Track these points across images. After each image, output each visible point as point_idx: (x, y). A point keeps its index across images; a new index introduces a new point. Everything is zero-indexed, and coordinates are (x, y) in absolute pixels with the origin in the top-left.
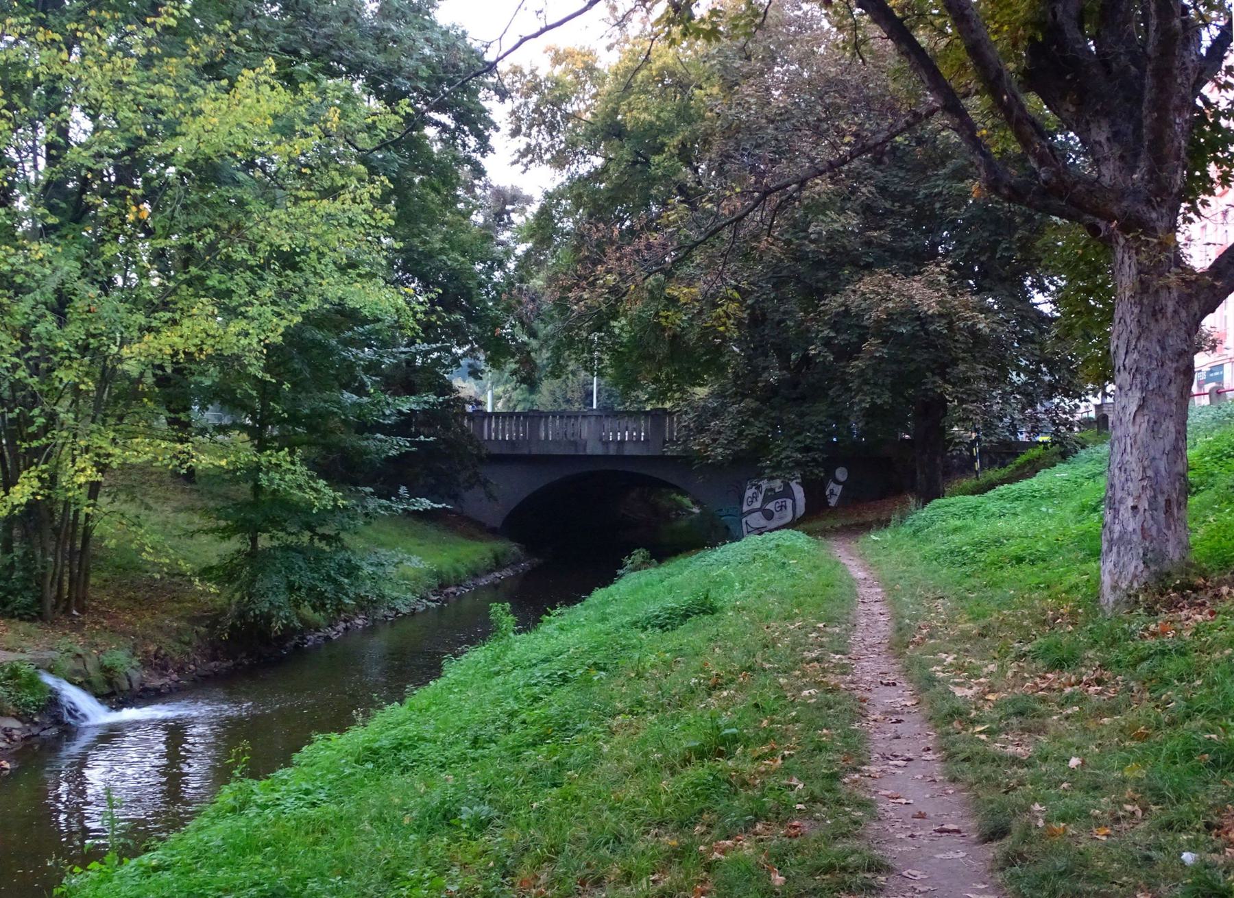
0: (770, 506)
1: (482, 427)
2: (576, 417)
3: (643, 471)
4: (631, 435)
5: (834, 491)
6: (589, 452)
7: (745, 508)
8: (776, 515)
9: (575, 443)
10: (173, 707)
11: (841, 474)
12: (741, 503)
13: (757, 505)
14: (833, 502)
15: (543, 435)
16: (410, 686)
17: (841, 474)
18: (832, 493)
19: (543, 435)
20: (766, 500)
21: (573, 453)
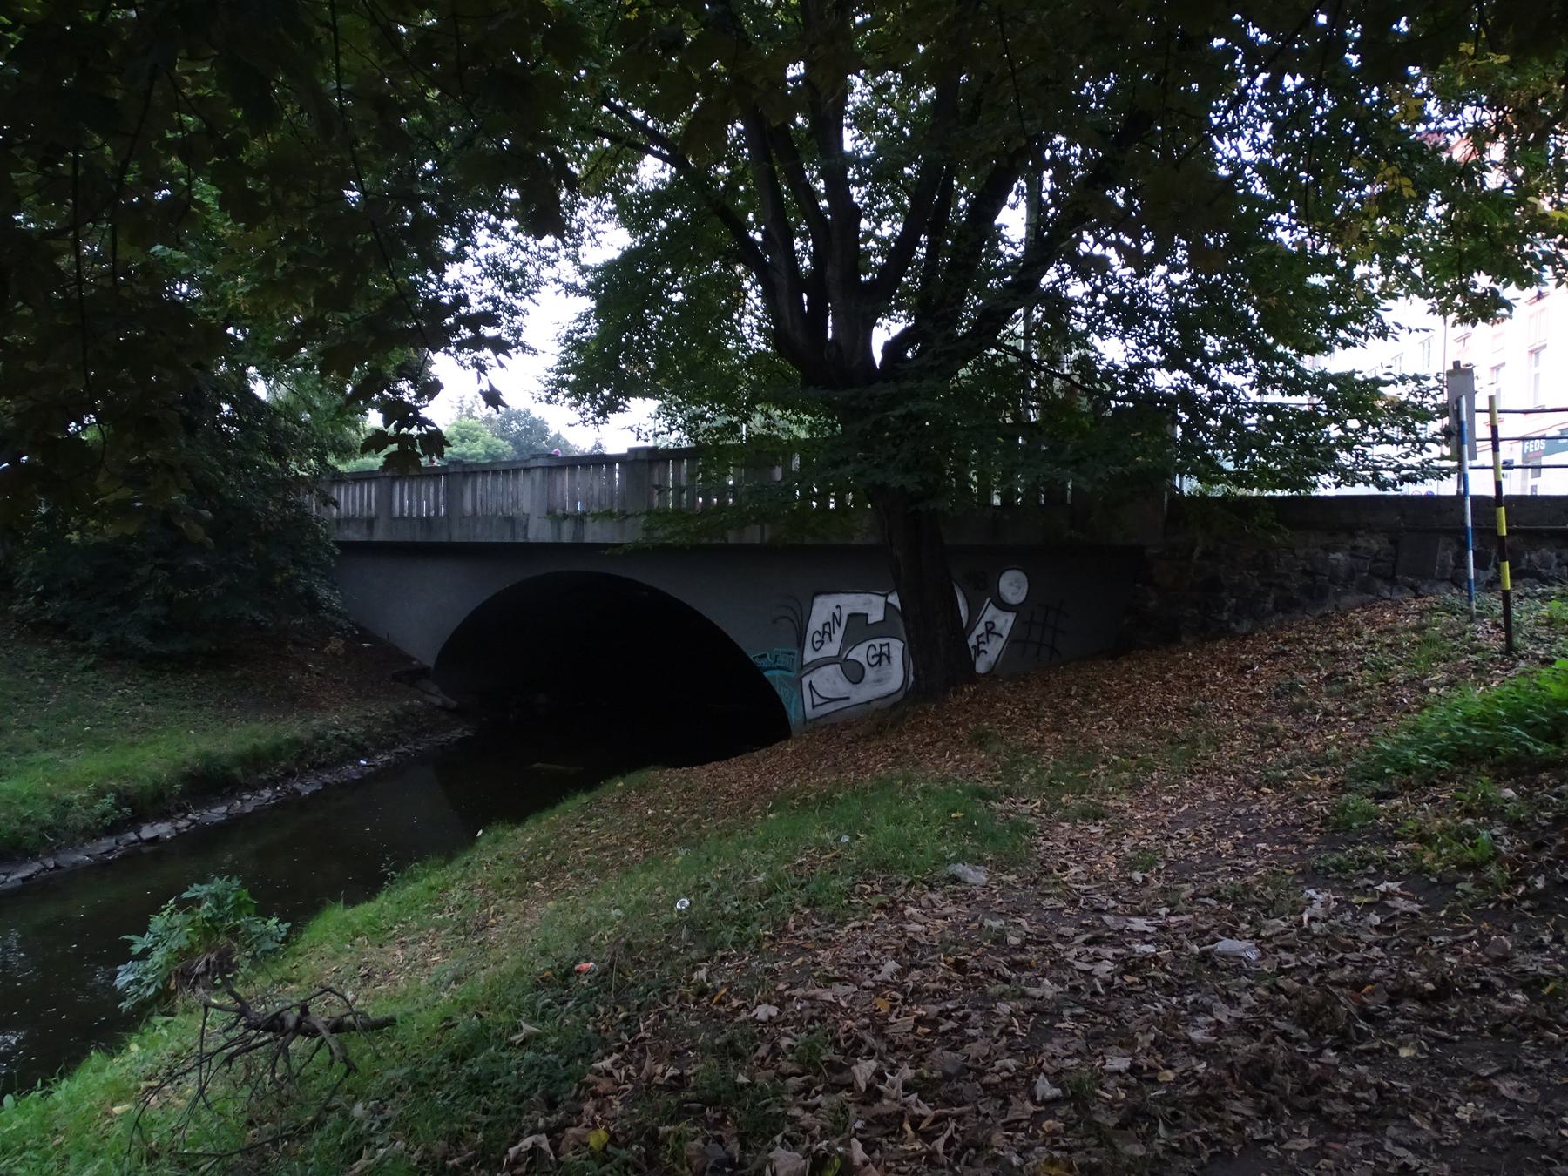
0: (859, 654)
1: (391, 497)
2: (516, 471)
3: (638, 578)
4: (707, 501)
5: (992, 632)
6: (532, 537)
7: (809, 656)
8: (870, 674)
9: (510, 520)
10: (293, 700)
11: (1013, 586)
12: (801, 644)
13: (831, 649)
14: (989, 655)
15: (468, 506)
16: (328, 901)
17: (1013, 586)
18: (990, 630)
19: (468, 506)
20: (850, 641)
21: (508, 539)
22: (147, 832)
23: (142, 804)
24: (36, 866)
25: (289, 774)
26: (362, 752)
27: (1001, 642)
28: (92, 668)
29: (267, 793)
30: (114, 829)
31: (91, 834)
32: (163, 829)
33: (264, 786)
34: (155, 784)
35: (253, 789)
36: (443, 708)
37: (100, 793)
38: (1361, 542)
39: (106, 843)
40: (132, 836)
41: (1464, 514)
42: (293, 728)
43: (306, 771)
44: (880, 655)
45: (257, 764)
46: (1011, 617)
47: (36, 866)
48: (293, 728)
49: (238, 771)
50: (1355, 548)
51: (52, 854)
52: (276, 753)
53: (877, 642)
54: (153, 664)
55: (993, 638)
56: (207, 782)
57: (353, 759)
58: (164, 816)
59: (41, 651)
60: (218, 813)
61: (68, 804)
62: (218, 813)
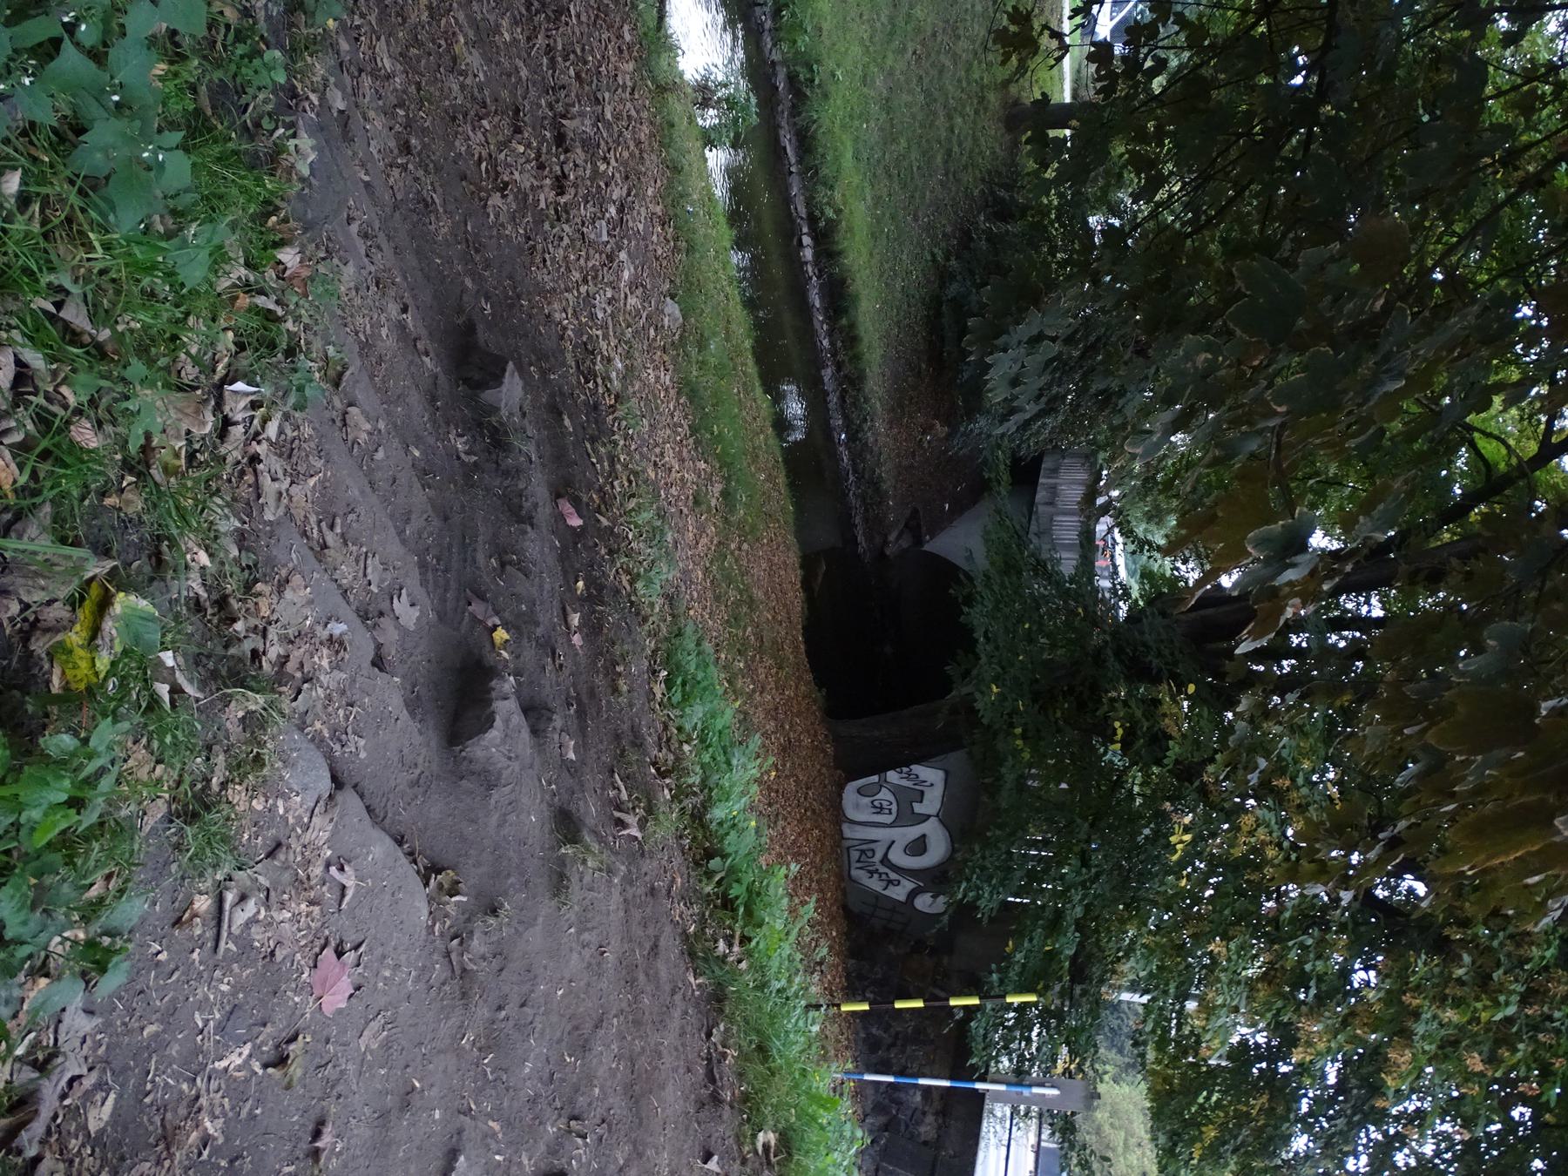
10: (899, 407)
22: (806, 240)
23: (825, 238)
24: (793, 160)
25: (839, 366)
26: (852, 438)
27: (879, 889)
28: (934, 260)
29: (826, 343)
30: (812, 220)
31: (809, 203)
32: (808, 254)
33: (831, 343)
34: (840, 253)
35: (830, 333)
36: (885, 542)
37: (838, 212)
38: (930, 1119)
39: (803, 211)
40: (805, 230)
41: (937, 1088)
42: (876, 385)
43: (840, 384)
44: (881, 808)
45: (850, 339)
46: (902, 898)
47: (793, 160)
48: (876, 385)
49: (844, 321)
50: (924, 1113)
51: (799, 174)
52: (857, 358)
53: (894, 808)
54: (935, 304)
55: (884, 884)
56: (838, 296)
57: (847, 427)
58: (816, 255)
59: (949, 229)
60: (816, 300)
61: (832, 188)
62: (816, 300)
